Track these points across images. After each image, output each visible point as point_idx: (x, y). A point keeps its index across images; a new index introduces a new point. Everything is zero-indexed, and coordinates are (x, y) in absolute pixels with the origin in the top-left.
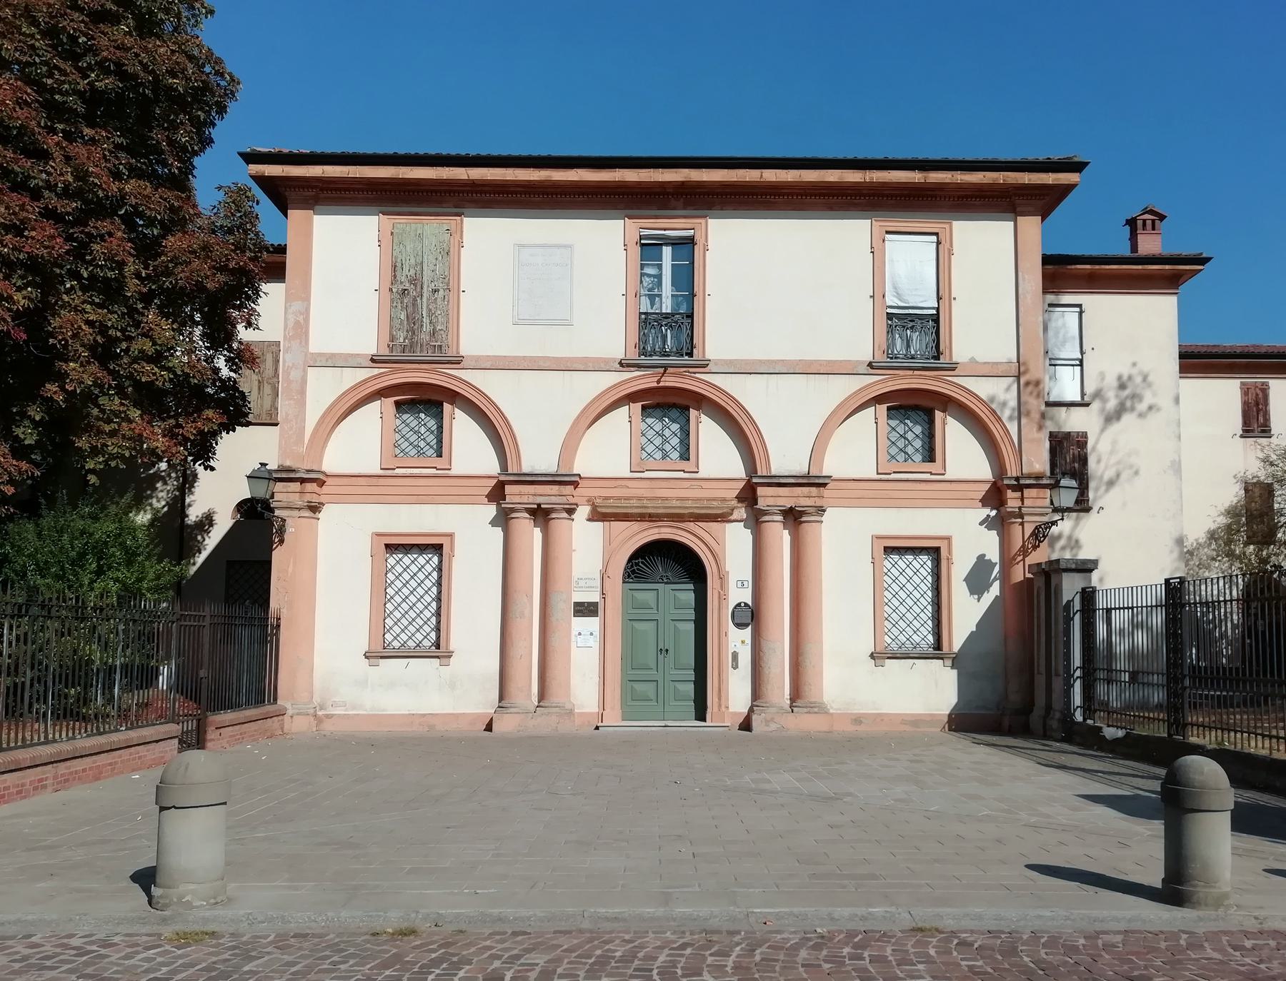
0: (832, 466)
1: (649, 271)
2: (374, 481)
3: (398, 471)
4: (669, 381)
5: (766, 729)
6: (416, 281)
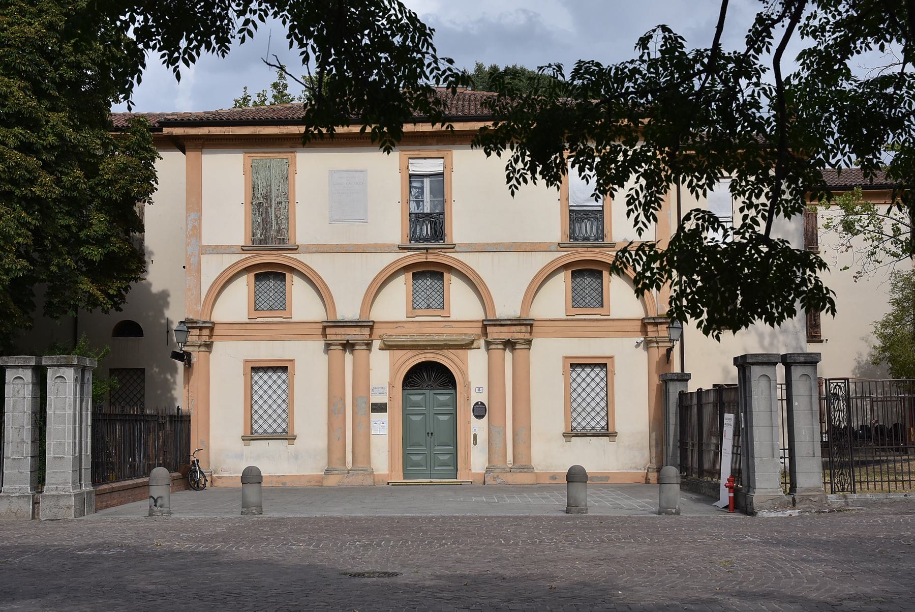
0: (538, 311)
1: (414, 184)
2: (243, 327)
3: (259, 320)
4: (431, 258)
5: (494, 483)
6: (267, 197)
